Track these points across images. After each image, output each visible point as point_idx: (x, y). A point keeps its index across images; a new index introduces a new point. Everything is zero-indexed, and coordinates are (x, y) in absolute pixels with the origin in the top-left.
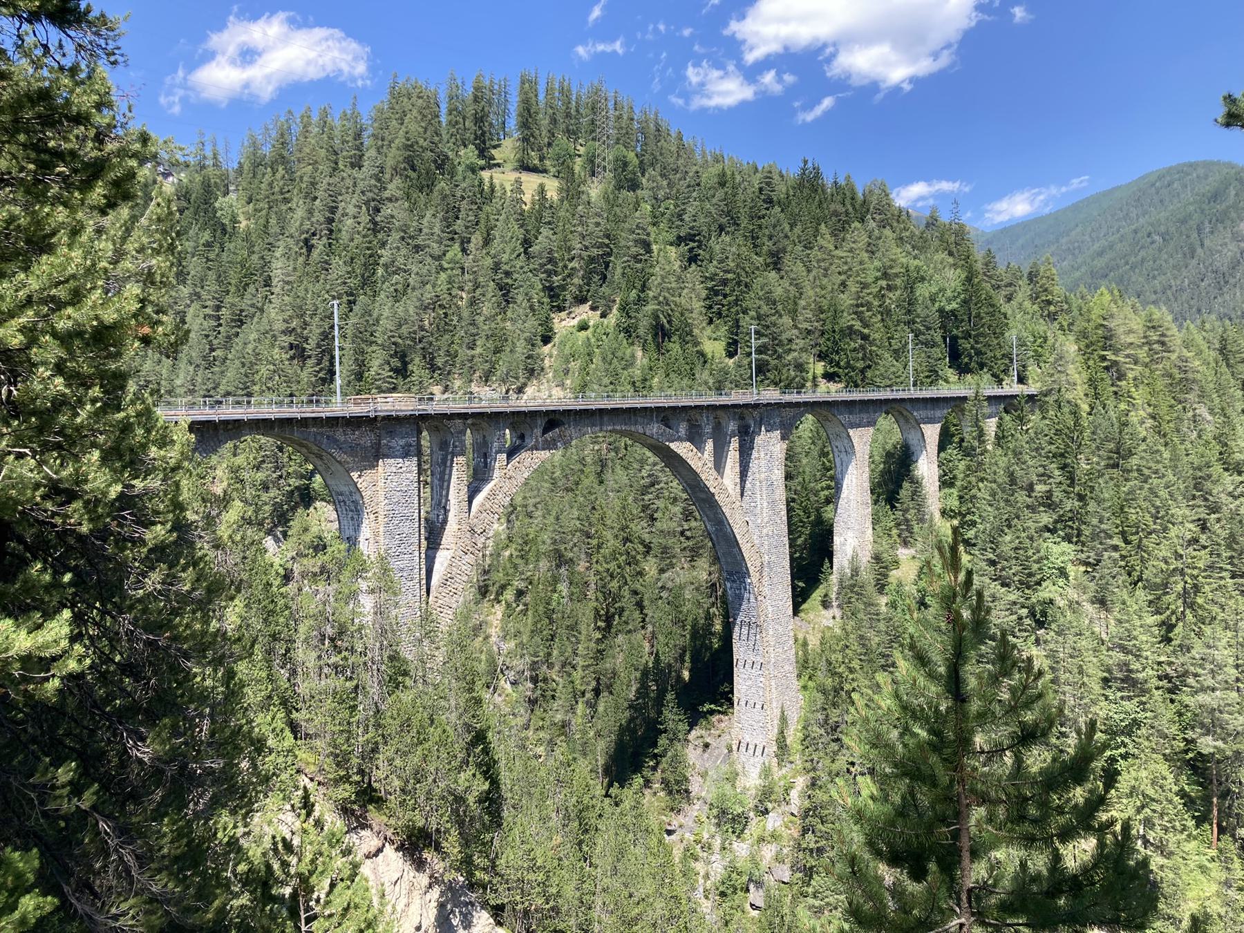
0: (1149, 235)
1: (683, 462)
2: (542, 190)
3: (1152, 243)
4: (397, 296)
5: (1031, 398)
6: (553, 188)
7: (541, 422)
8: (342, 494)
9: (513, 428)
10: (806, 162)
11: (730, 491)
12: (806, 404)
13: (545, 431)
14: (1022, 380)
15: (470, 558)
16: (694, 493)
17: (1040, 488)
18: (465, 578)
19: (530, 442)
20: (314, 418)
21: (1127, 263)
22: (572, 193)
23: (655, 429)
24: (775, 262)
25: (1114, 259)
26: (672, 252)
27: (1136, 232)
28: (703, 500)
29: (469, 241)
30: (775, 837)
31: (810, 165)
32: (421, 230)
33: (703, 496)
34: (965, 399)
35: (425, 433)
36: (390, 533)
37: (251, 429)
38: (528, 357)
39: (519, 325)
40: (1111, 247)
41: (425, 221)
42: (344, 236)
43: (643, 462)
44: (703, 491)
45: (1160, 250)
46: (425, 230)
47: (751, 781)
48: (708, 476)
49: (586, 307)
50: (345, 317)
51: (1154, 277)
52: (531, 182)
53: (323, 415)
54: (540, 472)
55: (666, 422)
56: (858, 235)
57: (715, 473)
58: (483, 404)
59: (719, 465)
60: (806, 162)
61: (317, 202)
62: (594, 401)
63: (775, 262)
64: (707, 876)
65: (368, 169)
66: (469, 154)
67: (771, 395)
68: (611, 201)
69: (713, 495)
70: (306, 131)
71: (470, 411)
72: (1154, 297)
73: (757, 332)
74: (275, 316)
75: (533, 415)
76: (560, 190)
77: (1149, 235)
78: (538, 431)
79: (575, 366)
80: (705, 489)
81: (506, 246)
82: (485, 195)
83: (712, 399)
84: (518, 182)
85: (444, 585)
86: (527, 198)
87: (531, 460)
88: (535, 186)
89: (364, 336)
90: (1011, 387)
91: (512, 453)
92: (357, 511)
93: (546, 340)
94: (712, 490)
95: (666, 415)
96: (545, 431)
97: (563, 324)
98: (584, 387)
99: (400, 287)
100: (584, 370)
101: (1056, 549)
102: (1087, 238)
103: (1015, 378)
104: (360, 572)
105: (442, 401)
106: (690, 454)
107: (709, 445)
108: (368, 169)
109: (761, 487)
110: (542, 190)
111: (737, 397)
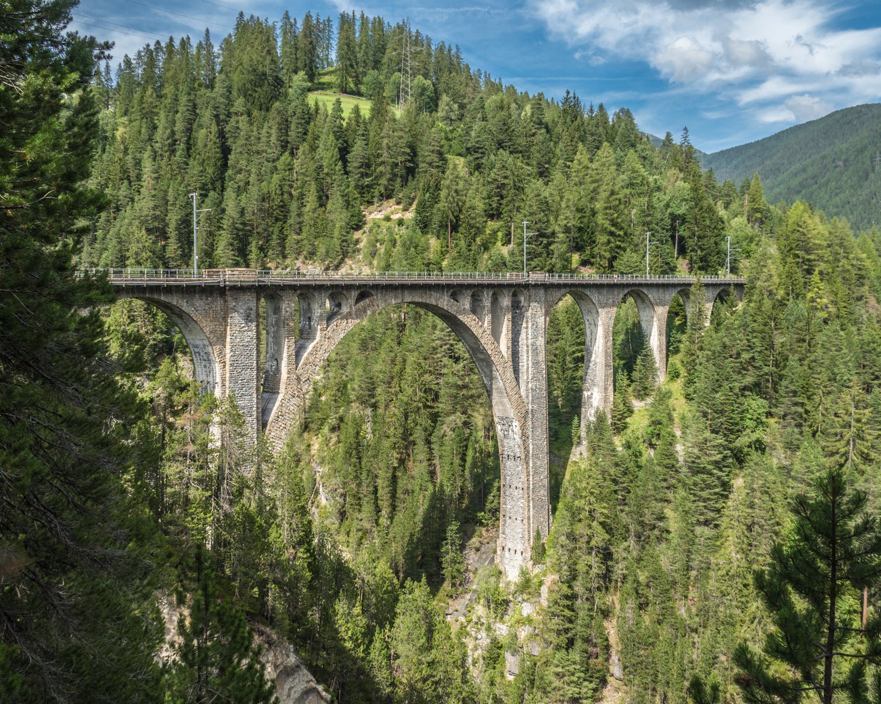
0: (834, 161)
1: (467, 329)
2: (356, 110)
3: (836, 167)
4: (239, 191)
5: (739, 286)
6: (366, 107)
7: (354, 294)
8: (197, 347)
9: (332, 297)
10: (568, 93)
11: (505, 355)
12: (565, 286)
13: (358, 301)
14: (734, 270)
15: (294, 401)
16: (474, 353)
17: (746, 356)
18: (292, 416)
19: (345, 310)
20: (177, 286)
21: (816, 183)
22: (379, 112)
23: (444, 302)
24: (544, 174)
25: (806, 180)
26: (461, 161)
27: (824, 158)
28: (482, 360)
29: (297, 149)
30: (529, 620)
31: (571, 95)
32: (259, 139)
33: (481, 356)
34: (690, 285)
35: (263, 300)
36: (234, 380)
37: (128, 293)
38: (343, 241)
39: (337, 215)
40: (804, 170)
41: (264, 131)
42: (200, 144)
43: (434, 327)
44: (482, 353)
45: (842, 174)
46: (264, 139)
47: (513, 576)
48: (486, 341)
49: (392, 201)
50: (199, 207)
51: (837, 195)
52: (348, 104)
53: (184, 284)
54: (350, 336)
55: (454, 296)
56: (606, 152)
57: (492, 339)
58: (307, 278)
59: (496, 334)
60: (568, 93)
61: (179, 115)
62: (397, 275)
63: (544, 174)
64: (476, 648)
65: (219, 88)
66: (299, 79)
67: (538, 277)
68: (413, 118)
69: (489, 356)
70: (592, 111)
71: (298, 283)
72: (835, 210)
73: (528, 228)
74: (145, 204)
75: (349, 287)
76: (373, 109)
77: (834, 161)
78: (352, 301)
79: (382, 249)
80: (484, 352)
81: (327, 152)
82: (309, 116)
83: (493, 279)
84: (338, 102)
85: (277, 420)
86: (346, 114)
87: (343, 328)
88: (353, 107)
89: (215, 222)
90: (725, 276)
91: (330, 318)
92: (209, 360)
93: (358, 227)
94: (490, 352)
95: (455, 290)
96: (358, 301)
97: (374, 215)
98: (388, 267)
99: (242, 184)
100: (388, 254)
101: (754, 404)
102: (785, 161)
103: (728, 270)
104: (213, 406)
105: (278, 275)
106: (473, 323)
107: (488, 319)
108: (219, 88)
109: (528, 351)
110: (356, 110)
111: (508, 277)
